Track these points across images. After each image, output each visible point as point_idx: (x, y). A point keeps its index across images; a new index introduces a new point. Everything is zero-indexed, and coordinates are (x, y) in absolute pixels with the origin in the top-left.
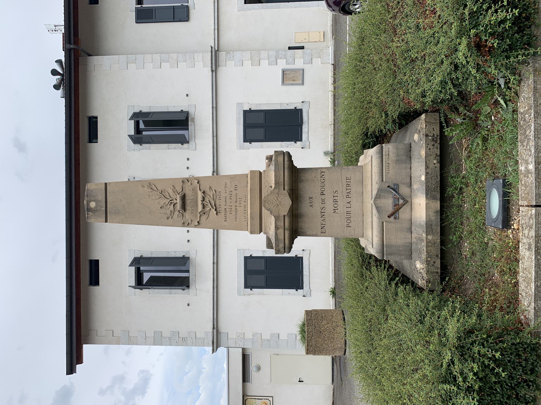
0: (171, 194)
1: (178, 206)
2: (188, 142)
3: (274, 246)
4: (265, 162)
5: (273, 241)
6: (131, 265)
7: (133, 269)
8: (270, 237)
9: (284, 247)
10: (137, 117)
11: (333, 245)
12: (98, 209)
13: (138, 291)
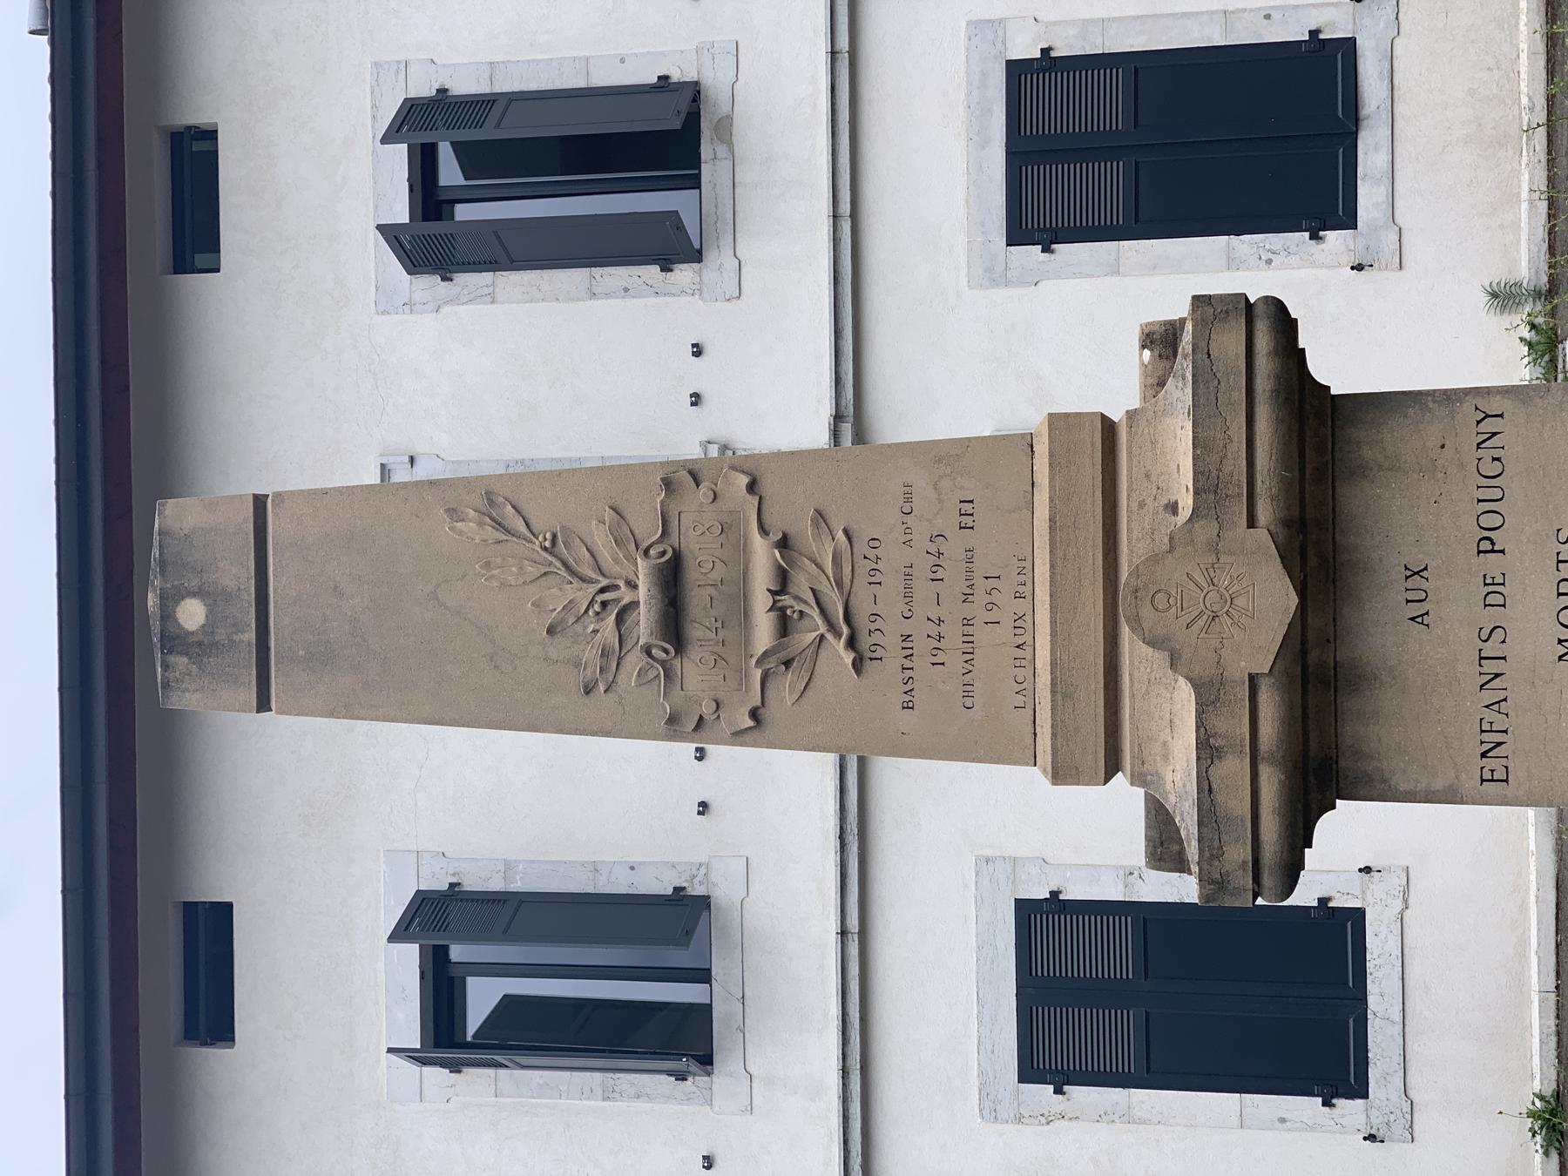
1: (645, 623)
2: (697, 256)
3: (1192, 851)
4: (1133, 360)
5: (1188, 825)
6: (400, 934)
7: (410, 953)
8: (1171, 802)
9: (1256, 862)
10: (424, 122)
11: (1549, 844)
12: (221, 635)
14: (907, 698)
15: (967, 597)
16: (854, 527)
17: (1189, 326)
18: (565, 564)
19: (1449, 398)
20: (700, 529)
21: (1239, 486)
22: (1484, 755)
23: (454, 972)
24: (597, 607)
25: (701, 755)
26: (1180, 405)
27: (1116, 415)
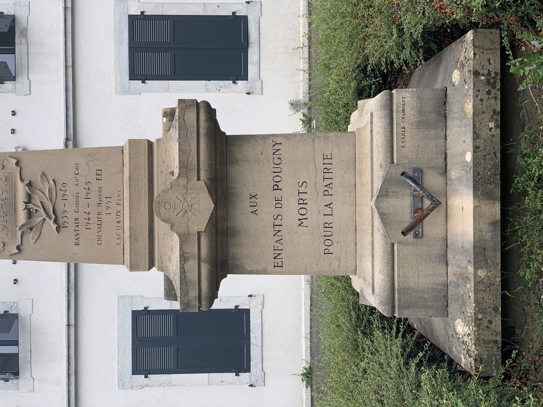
2: (14, 79)
4: (160, 121)
5: (177, 284)
8: (171, 276)
14: (77, 241)
15: (99, 205)
16: (57, 179)
17: (177, 110)
19: (264, 137)
21: (194, 166)
22: (275, 258)
25: (14, 263)
26: (175, 137)
27: (153, 140)
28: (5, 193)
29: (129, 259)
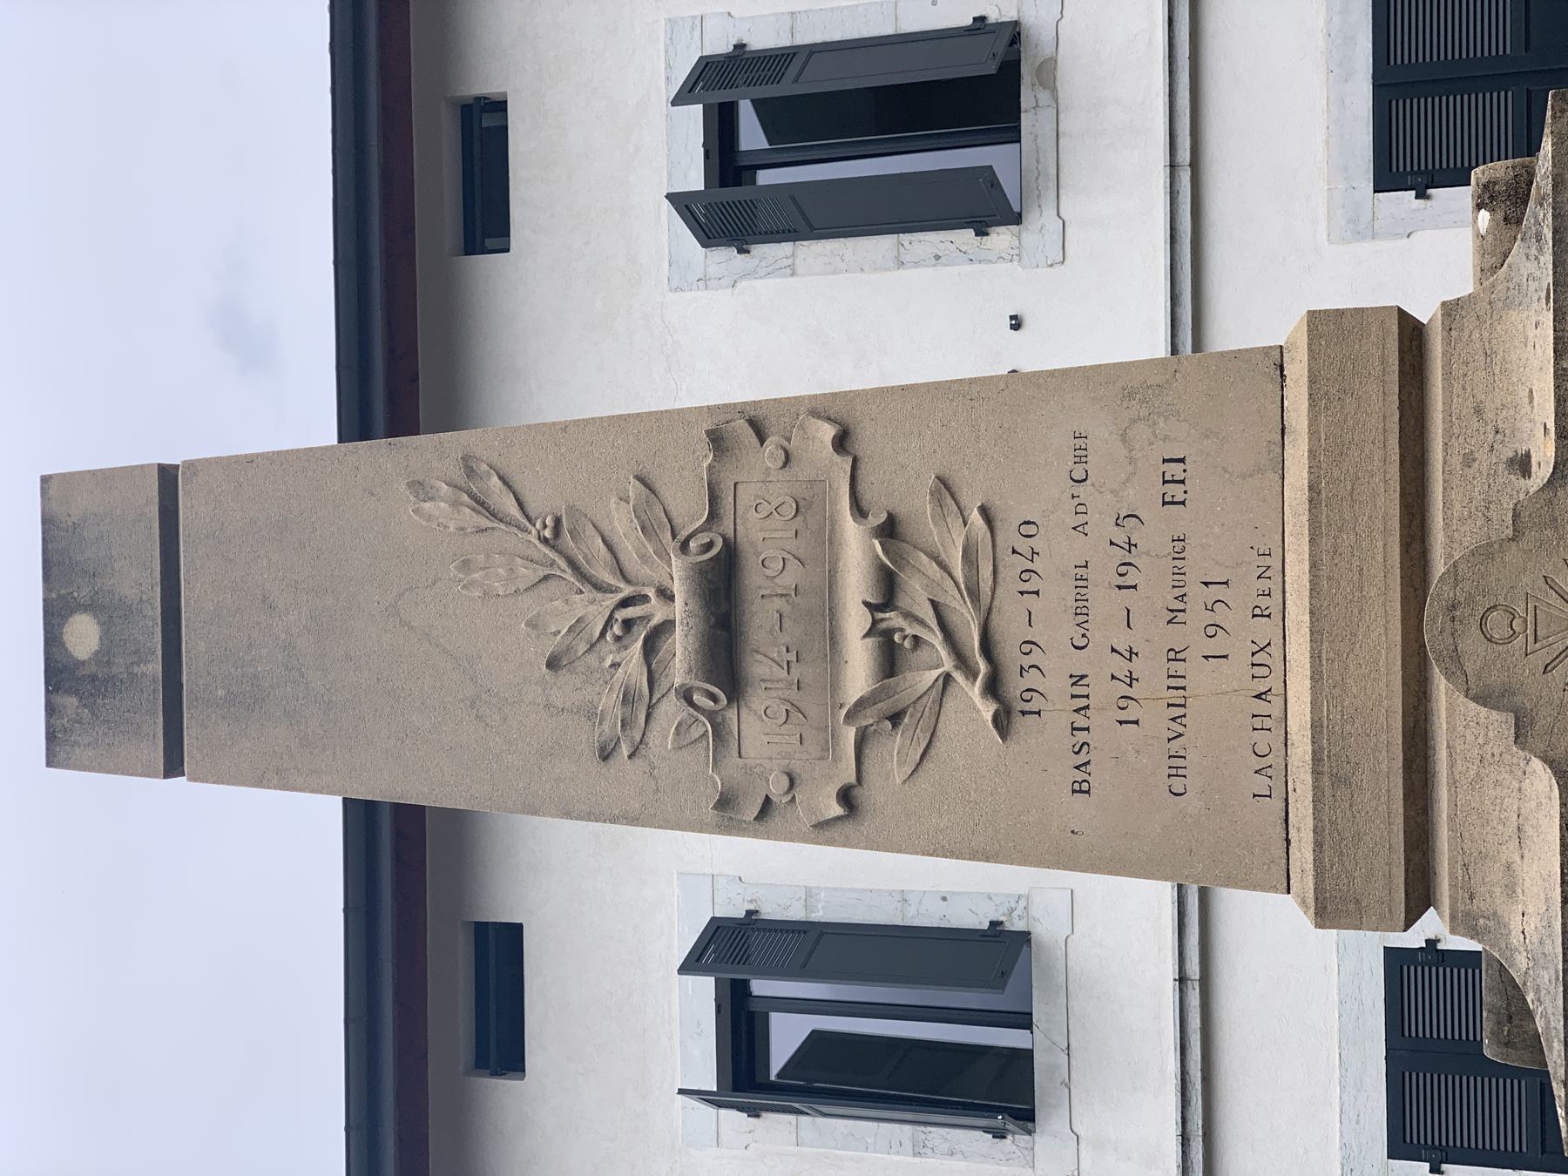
0: (630, 544)
1: (681, 650)
2: (1016, 219)
6: (692, 965)
7: (704, 988)
10: (719, 82)
12: (119, 667)
13: (733, 1119)
14: (1080, 776)
15: (1174, 616)
16: (997, 503)
18: (572, 563)
20: (765, 509)
23: (755, 1007)
24: (617, 629)
27: (1424, 311)
28: (793, 565)
29: (1310, 866)
